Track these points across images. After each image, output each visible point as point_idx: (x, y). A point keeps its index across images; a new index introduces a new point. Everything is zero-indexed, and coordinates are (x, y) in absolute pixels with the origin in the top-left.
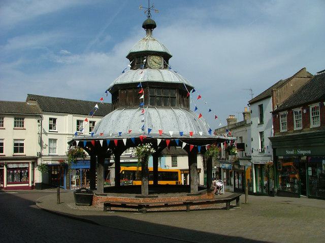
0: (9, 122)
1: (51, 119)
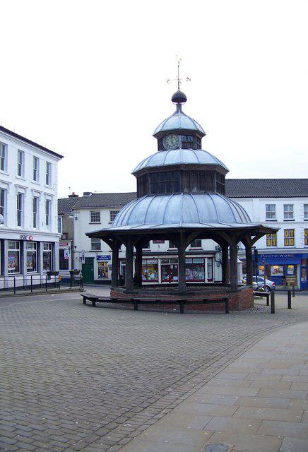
0: (105, 215)
1: (285, 206)
